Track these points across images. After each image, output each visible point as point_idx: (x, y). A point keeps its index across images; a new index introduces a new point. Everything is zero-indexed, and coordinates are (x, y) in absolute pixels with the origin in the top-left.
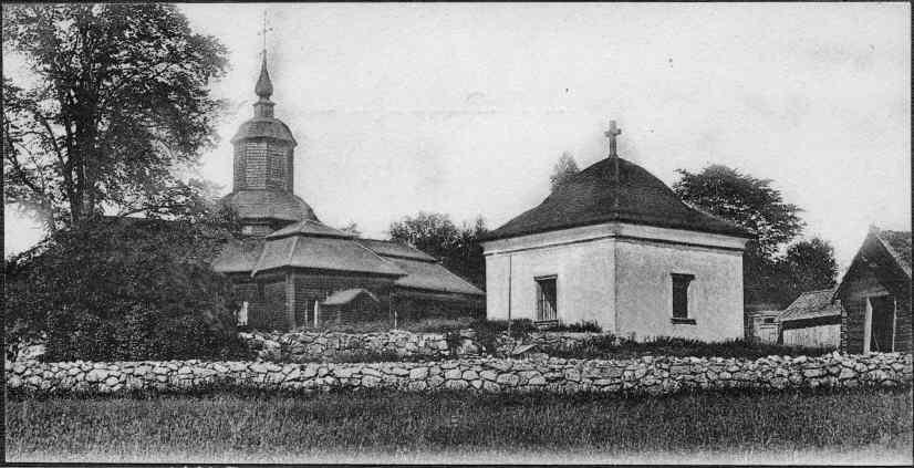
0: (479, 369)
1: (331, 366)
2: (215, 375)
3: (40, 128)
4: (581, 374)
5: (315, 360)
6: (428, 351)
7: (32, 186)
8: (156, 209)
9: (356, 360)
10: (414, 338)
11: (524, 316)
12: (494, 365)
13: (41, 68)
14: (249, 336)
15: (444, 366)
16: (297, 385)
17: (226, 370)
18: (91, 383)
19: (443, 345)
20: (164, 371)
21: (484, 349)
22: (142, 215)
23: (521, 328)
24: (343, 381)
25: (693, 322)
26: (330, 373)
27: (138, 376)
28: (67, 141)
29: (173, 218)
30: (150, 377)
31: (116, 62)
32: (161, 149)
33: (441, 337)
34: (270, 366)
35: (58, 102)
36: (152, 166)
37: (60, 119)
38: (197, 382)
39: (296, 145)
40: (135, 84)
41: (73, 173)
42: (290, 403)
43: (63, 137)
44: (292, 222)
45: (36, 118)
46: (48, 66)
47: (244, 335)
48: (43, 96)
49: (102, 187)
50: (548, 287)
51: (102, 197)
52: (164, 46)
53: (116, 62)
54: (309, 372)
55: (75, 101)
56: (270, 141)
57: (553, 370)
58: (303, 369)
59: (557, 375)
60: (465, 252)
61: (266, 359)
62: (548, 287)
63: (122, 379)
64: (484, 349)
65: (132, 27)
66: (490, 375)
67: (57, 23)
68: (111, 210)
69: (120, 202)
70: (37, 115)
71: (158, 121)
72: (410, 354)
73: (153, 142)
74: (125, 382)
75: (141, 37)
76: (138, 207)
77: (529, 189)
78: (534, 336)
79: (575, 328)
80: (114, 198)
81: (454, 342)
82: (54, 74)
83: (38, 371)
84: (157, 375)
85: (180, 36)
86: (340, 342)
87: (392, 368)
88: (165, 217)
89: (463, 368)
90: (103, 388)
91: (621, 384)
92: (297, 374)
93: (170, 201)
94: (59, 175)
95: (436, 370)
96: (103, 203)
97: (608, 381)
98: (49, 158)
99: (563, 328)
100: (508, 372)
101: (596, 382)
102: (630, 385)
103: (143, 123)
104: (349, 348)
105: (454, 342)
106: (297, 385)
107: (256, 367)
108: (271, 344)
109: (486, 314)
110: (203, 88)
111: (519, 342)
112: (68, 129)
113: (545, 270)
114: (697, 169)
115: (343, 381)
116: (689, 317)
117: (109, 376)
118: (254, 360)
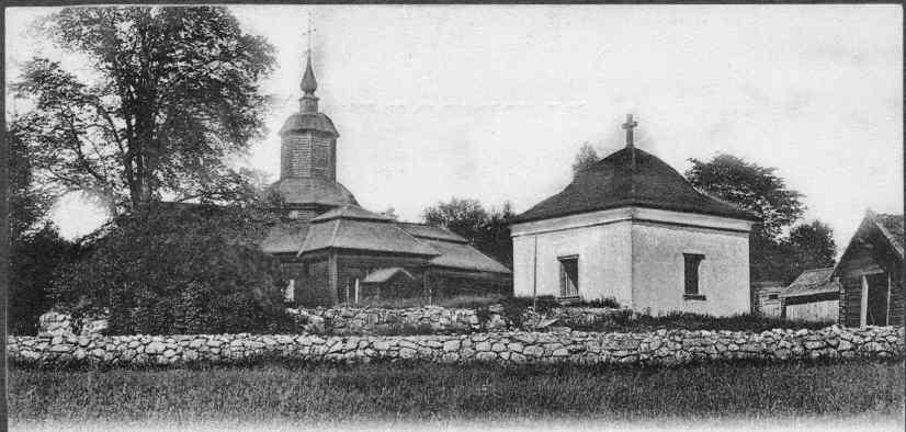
0: (507, 341)
1: (371, 339)
2: (264, 348)
3: (102, 121)
4: (602, 346)
5: (357, 334)
6: (460, 325)
7: (95, 174)
8: (209, 195)
9: (394, 333)
10: (447, 313)
11: (548, 293)
12: (520, 338)
13: (103, 66)
14: (295, 311)
15: (475, 339)
16: (340, 356)
17: (274, 342)
18: (150, 355)
19: (474, 319)
20: (217, 344)
21: (511, 323)
22: (197, 201)
23: (546, 304)
24: (382, 353)
25: (703, 298)
26: (370, 346)
27: (193, 348)
28: (128, 133)
29: (225, 203)
30: (206, 349)
31: (171, 60)
32: (214, 140)
33: (472, 312)
34: (315, 339)
35: (119, 98)
36: (206, 156)
37: (120, 113)
38: (247, 354)
39: (338, 136)
40: (191, 80)
41: (133, 162)
42: (334, 373)
43: (123, 130)
44: (336, 207)
45: (98, 112)
46: (110, 65)
47: (290, 310)
48: (106, 92)
49: (160, 175)
50: (570, 266)
51: (159, 184)
52: (216, 46)
53: (171, 60)
54: (351, 344)
55: (135, 96)
56: (315, 133)
57: (575, 343)
58: (344, 341)
59: (579, 347)
60: (494, 234)
61: (311, 333)
62: (570, 266)
63: (179, 351)
64: (511, 323)
65: (187, 28)
66: (517, 347)
67: (118, 25)
68: (168, 196)
69: (176, 189)
70: (100, 109)
71: (211, 115)
72: (443, 327)
73: (207, 134)
74: (181, 354)
75: (195, 37)
76: (193, 193)
77: (555, 176)
78: (558, 311)
79: (595, 304)
80: (171, 185)
81: (484, 316)
82: (115, 72)
83: (102, 344)
84: (211, 347)
85: (231, 36)
86: (379, 317)
87: (426, 341)
88: (217, 203)
89: (492, 341)
90: (161, 359)
91: (638, 355)
92: (339, 346)
93: (222, 188)
94: (120, 164)
95: (467, 343)
96: (161, 190)
97: (625, 353)
98: (112, 149)
99: (584, 304)
100: (534, 344)
101: (615, 354)
102: (646, 357)
103: (198, 116)
104: (387, 322)
105: (484, 316)
106: (340, 356)
107: (302, 339)
108: (316, 318)
109: (512, 290)
110: (252, 84)
111: (544, 317)
112: (128, 122)
113: (566, 251)
114: (707, 158)
115: (382, 353)
116: (700, 293)
117: (167, 349)
118: (300, 334)
